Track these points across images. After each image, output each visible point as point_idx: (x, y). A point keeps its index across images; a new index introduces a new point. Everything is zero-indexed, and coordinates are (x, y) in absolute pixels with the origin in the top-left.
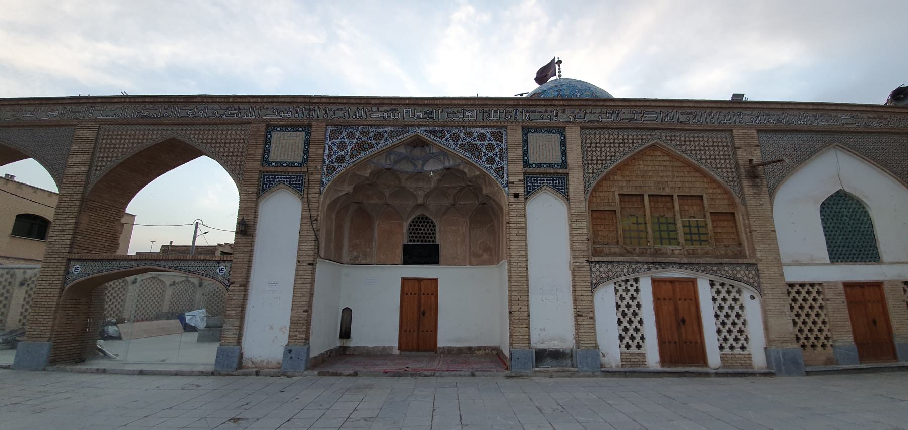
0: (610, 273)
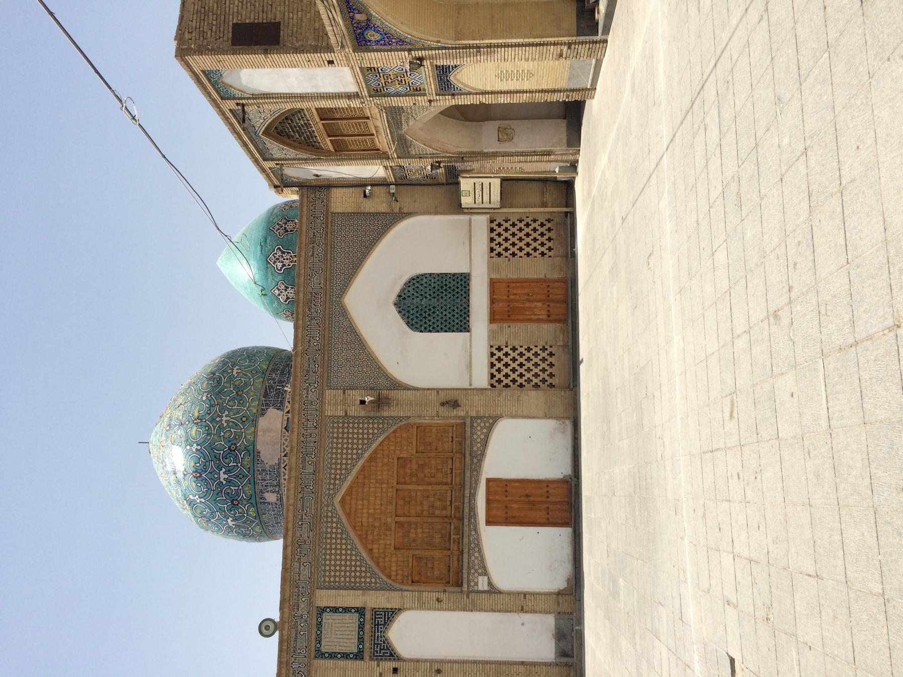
0: (480, 571)
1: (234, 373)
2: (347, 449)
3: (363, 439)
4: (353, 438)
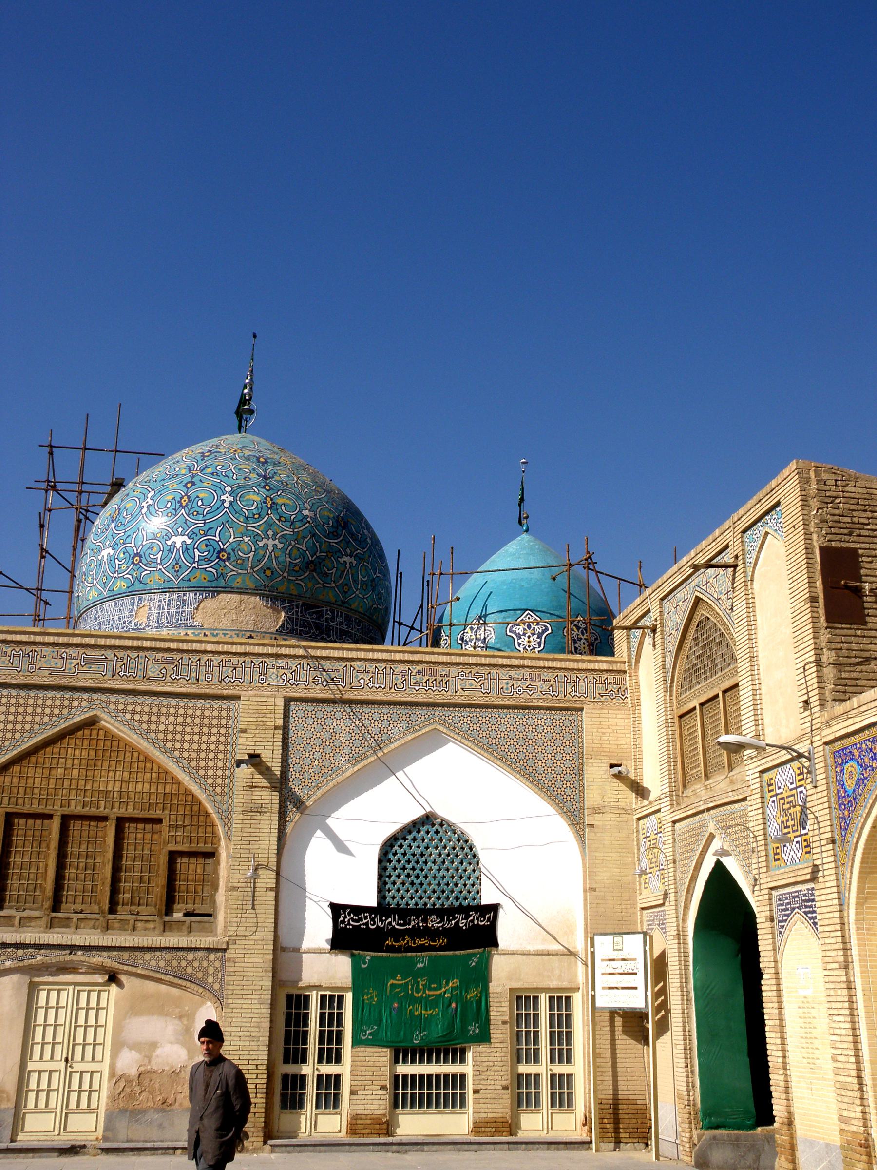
1: (345, 558)
2: (183, 733)
3: (198, 759)
4: (200, 742)
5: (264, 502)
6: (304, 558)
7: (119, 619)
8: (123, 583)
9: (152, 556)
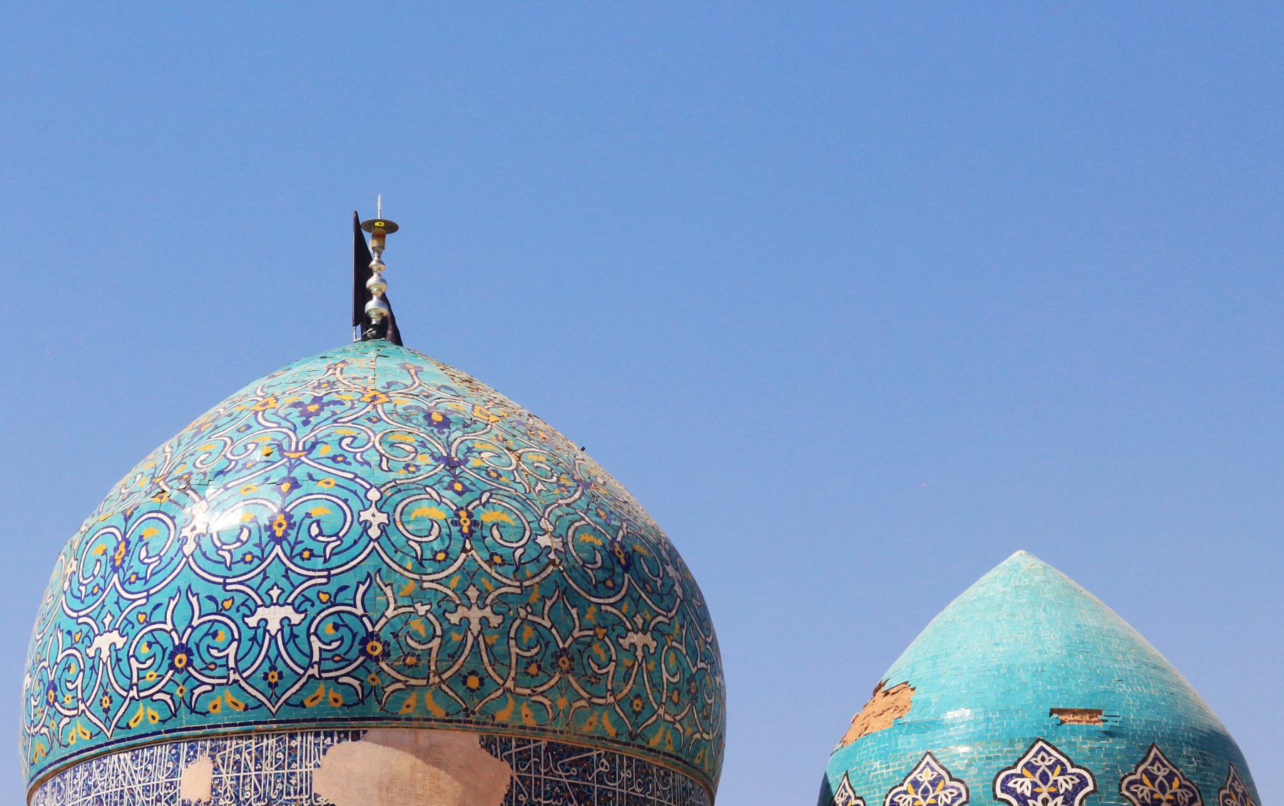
1: (635, 638)
5: (455, 523)
6: (547, 645)
7: (146, 790)
8: (150, 712)
9: (214, 652)
